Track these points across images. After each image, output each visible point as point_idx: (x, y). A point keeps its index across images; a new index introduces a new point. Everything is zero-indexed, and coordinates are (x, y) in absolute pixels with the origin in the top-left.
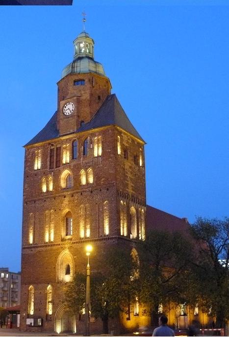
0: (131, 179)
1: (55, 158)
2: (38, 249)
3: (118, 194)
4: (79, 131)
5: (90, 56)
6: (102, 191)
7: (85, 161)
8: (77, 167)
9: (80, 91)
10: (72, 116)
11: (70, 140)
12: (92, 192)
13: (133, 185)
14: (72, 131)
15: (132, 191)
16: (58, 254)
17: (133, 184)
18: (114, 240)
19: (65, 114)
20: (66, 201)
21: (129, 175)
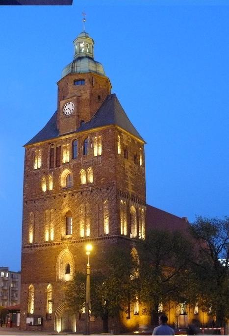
0: (131, 178)
1: (55, 157)
2: (38, 248)
3: (118, 194)
4: (79, 130)
5: (90, 56)
6: (102, 190)
7: (85, 160)
8: (77, 167)
9: (80, 90)
10: (72, 115)
12: (92, 191)
13: (133, 185)
14: (72, 131)
15: (132, 191)
16: (58, 253)
17: (133, 183)
18: (114, 239)
19: (65, 113)
20: (66, 201)
21: (129, 175)
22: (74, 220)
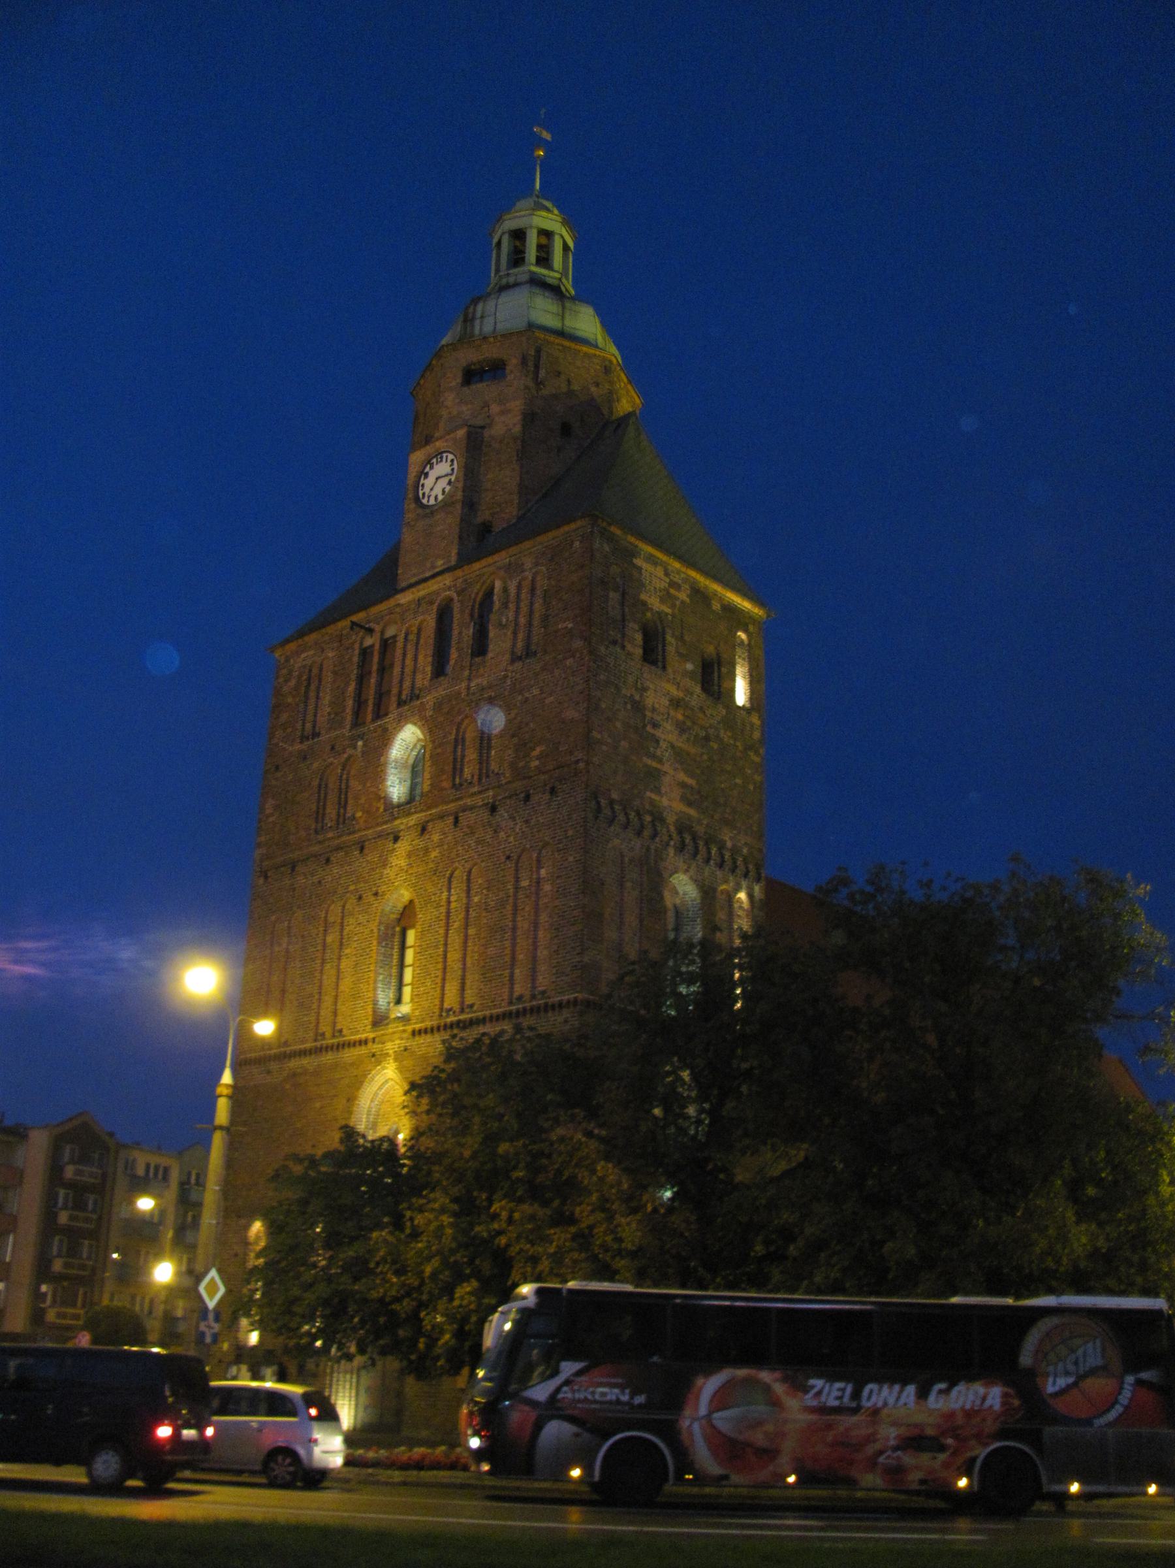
0: (678, 754)
3: (599, 809)
4: (465, 559)
6: (535, 799)
7: (479, 680)
9: (486, 405)
10: (446, 504)
11: (431, 603)
13: (691, 782)
14: (440, 564)
15: (681, 807)
16: (358, 1082)
17: (692, 776)
18: (566, 1013)
19: (425, 501)
20: (399, 856)
21: (668, 734)
22: (421, 936)
